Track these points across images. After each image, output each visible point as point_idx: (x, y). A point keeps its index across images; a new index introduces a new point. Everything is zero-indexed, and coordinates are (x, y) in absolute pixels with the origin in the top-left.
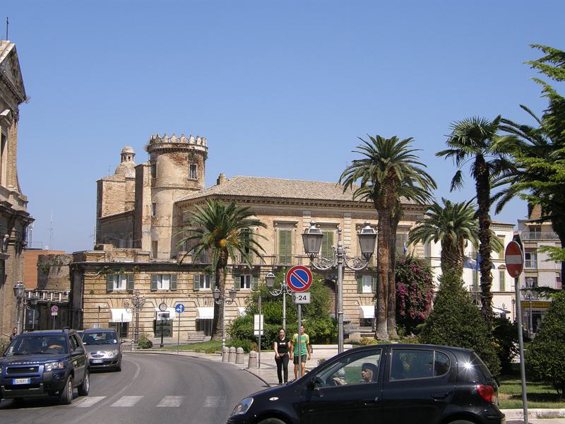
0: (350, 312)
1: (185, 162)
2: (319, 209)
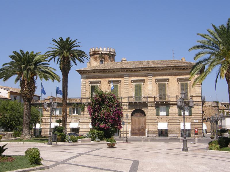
0: (152, 126)
1: (98, 59)
2: (133, 73)
